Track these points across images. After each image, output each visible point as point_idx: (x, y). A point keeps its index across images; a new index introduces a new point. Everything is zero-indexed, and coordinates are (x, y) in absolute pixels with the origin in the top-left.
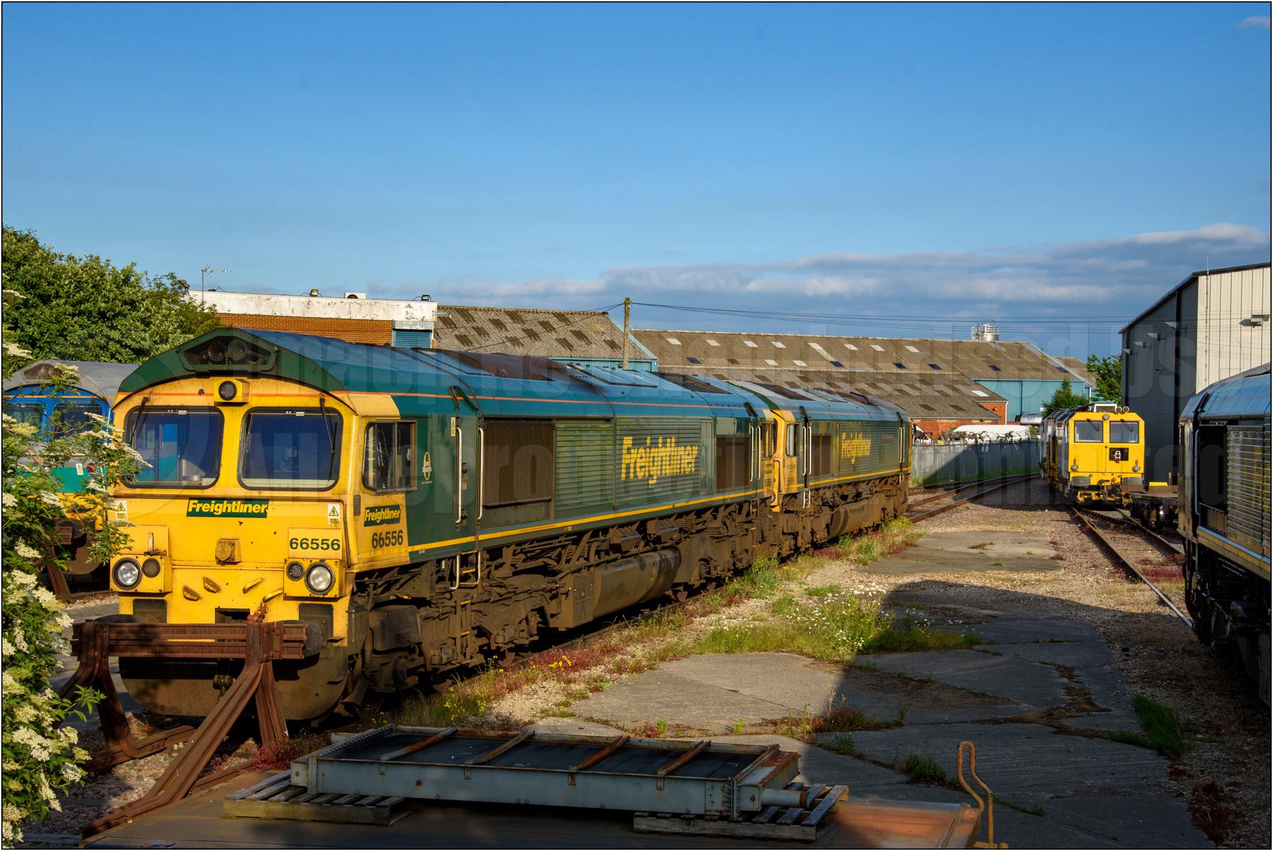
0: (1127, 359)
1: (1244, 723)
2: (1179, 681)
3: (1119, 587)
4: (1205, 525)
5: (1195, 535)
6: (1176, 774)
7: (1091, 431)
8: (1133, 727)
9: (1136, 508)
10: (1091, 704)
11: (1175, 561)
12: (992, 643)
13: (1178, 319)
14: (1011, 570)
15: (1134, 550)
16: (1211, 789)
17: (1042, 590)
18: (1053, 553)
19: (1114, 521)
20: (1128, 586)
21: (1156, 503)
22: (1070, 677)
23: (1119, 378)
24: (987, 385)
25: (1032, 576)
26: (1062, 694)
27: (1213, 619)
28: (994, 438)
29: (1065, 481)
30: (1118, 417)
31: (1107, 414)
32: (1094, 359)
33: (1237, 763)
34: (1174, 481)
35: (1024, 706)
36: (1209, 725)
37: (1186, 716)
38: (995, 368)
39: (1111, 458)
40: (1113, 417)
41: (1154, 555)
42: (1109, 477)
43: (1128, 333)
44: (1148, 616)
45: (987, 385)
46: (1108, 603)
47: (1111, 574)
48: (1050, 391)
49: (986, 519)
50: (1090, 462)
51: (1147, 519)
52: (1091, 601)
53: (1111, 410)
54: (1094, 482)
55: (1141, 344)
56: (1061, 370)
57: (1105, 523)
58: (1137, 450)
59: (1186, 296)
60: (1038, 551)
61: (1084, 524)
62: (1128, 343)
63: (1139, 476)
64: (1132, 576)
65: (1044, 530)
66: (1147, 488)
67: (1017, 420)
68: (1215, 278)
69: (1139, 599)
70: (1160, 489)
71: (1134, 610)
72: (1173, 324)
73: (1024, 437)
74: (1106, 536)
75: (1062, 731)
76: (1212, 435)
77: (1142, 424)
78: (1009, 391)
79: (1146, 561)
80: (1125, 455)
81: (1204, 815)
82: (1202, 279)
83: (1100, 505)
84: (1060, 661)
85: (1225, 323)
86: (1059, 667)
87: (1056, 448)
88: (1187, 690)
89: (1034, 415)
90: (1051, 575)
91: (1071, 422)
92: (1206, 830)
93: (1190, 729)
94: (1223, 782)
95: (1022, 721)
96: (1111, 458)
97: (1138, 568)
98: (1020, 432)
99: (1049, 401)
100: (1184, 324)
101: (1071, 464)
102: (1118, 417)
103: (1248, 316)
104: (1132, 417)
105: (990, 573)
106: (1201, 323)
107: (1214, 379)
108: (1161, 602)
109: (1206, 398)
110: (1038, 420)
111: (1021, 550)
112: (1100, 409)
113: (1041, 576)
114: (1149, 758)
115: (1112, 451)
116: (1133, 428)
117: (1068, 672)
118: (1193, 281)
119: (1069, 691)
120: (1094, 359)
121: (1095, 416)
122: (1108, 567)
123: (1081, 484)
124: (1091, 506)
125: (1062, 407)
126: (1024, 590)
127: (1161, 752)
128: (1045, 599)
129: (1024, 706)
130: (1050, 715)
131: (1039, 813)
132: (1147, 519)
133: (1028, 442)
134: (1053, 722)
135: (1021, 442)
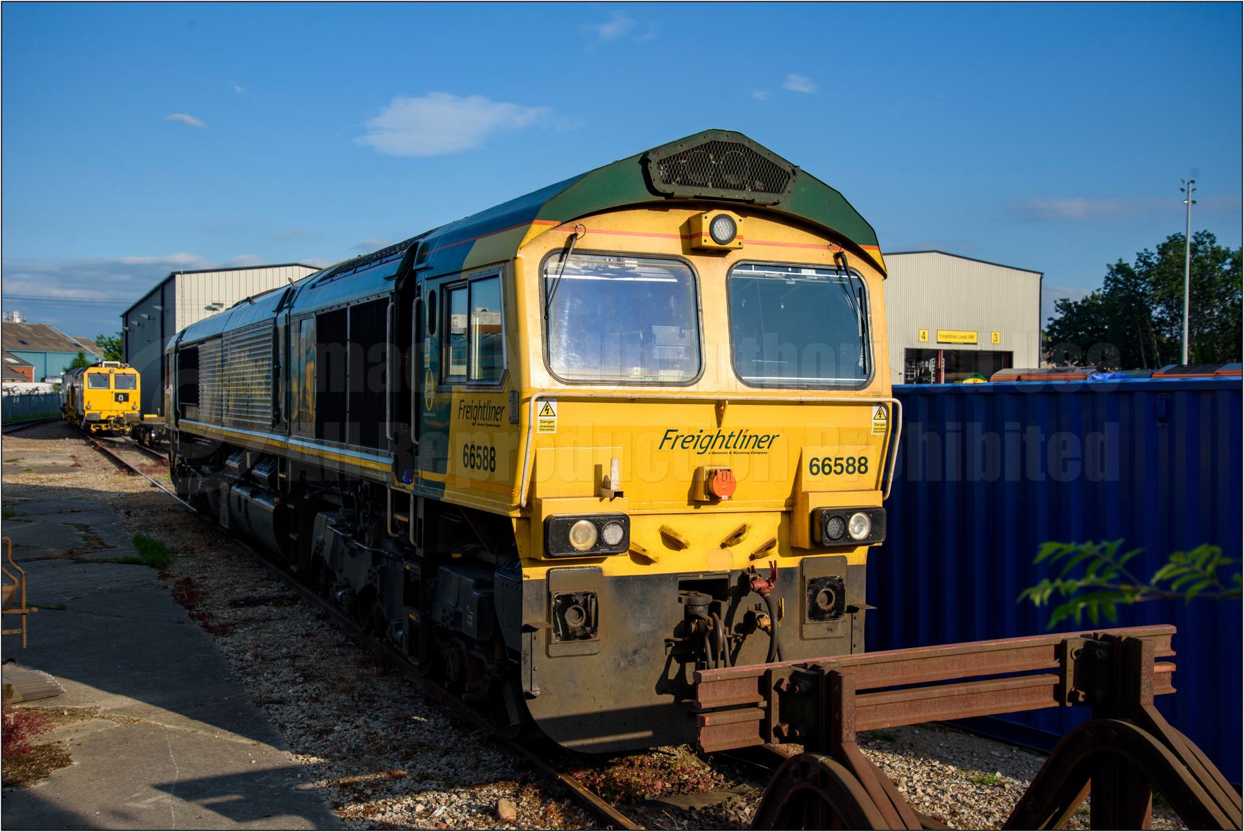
0: (126, 334)
1: (210, 545)
2: (169, 527)
3: (122, 478)
4: (184, 417)
5: (177, 425)
6: (163, 576)
7: (100, 381)
8: (135, 554)
9: (134, 434)
10: (102, 543)
11: (163, 464)
12: (24, 515)
13: (163, 304)
14: (40, 473)
15: (133, 459)
16: (188, 581)
17: (64, 484)
18: (73, 463)
19: (120, 443)
20: (129, 478)
21: (149, 429)
22: (87, 531)
23: (120, 352)
24: (18, 355)
25: (57, 476)
26: (81, 541)
27: (188, 118)
28: (24, 392)
29: (81, 417)
30: (121, 371)
31: (112, 369)
32: (102, 337)
33: (205, 567)
34: (162, 414)
35: (51, 550)
36: (186, 549)
37: (169, 545)
38: (23, 343)
39: (116, 400)
40: (117, 371)
41: (148, 462)
42: (115, 414)
43: (126, 316)
44: (144, 493)
45: (18, 355)
46: (117, 489)
47: (117, 473)
48: (68, 360)
49: (18, 445)
50: (100, 403)
51: (141, 437)
52: (103, 488)
53: (116, 366)
54: (103, 417)
55: (136, 323)
56: (77, 345)
57: (112, 445)
58: (135, 395)
59: (167, 289)
60: (61, 462)
61: (96, 445)
62: (126, 323)
63: (137, 412)
64: (131, 471)
65: (66, 450)
66: (142, 419)
67: (43, 380)
68: (187, 276)
69: (138, 485)
70: (150, 419)
71: (134, 491)
72: (159, 308)
73: (48, 391)
74: (114, 452)
75: (78, 561)
76: (189, 357)
77: (138, 375)
78: (36, 361)
79: (143, 465)
80: (126, 398)
81: (183, 596)
82: (178, 277)
83: (109, 433)
84: (78, 522)
85: (195, 307)
86: (77, 526)
87: (74, 396)
88: (172, 531)
89: (56, 377)
90: (71, 475)
91: (86, 374)
92: (183, 604)
93: (174, 552)
94: (196, 578)
95: (48, 558)
96: (116, 400)
97: (137, 469)
98: (45, 388)
99: (68, 366)
100: (166, 307)
101: (85, 404)
102: (121, 371)
103: (210, 304)
104: (130, 371)
105: (21, 475)
106: (178, 307)
107: (187, 325)
108: (153, 485)
109: (183, 332)
110: (60, 381)
111: (48, 462)
112: (107, 365)
113: (64, 475)
114: (145, 570)
115: (117, 395)
116: (131, 379)
117: (86, 528)
118: (172, 278)
119: (85, 538)
120: (102, 337)
121: (103, 370)
122: (114, 468)
123: (94, 418)
124: (100, 434)
125: (79, 366)
126: (50, 484)
127: (153, 565)
128: (67, 489)
129: (51, 550)
130: (71, 552)
131: (62, 608)
132: (141, 437)
133: (51, 395)
134: (74, 557)
135: (46, 395)
